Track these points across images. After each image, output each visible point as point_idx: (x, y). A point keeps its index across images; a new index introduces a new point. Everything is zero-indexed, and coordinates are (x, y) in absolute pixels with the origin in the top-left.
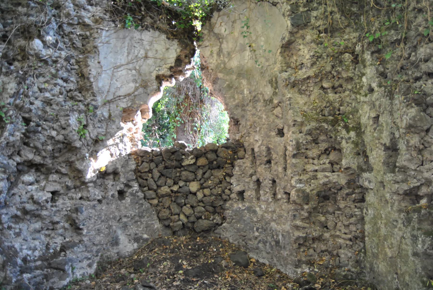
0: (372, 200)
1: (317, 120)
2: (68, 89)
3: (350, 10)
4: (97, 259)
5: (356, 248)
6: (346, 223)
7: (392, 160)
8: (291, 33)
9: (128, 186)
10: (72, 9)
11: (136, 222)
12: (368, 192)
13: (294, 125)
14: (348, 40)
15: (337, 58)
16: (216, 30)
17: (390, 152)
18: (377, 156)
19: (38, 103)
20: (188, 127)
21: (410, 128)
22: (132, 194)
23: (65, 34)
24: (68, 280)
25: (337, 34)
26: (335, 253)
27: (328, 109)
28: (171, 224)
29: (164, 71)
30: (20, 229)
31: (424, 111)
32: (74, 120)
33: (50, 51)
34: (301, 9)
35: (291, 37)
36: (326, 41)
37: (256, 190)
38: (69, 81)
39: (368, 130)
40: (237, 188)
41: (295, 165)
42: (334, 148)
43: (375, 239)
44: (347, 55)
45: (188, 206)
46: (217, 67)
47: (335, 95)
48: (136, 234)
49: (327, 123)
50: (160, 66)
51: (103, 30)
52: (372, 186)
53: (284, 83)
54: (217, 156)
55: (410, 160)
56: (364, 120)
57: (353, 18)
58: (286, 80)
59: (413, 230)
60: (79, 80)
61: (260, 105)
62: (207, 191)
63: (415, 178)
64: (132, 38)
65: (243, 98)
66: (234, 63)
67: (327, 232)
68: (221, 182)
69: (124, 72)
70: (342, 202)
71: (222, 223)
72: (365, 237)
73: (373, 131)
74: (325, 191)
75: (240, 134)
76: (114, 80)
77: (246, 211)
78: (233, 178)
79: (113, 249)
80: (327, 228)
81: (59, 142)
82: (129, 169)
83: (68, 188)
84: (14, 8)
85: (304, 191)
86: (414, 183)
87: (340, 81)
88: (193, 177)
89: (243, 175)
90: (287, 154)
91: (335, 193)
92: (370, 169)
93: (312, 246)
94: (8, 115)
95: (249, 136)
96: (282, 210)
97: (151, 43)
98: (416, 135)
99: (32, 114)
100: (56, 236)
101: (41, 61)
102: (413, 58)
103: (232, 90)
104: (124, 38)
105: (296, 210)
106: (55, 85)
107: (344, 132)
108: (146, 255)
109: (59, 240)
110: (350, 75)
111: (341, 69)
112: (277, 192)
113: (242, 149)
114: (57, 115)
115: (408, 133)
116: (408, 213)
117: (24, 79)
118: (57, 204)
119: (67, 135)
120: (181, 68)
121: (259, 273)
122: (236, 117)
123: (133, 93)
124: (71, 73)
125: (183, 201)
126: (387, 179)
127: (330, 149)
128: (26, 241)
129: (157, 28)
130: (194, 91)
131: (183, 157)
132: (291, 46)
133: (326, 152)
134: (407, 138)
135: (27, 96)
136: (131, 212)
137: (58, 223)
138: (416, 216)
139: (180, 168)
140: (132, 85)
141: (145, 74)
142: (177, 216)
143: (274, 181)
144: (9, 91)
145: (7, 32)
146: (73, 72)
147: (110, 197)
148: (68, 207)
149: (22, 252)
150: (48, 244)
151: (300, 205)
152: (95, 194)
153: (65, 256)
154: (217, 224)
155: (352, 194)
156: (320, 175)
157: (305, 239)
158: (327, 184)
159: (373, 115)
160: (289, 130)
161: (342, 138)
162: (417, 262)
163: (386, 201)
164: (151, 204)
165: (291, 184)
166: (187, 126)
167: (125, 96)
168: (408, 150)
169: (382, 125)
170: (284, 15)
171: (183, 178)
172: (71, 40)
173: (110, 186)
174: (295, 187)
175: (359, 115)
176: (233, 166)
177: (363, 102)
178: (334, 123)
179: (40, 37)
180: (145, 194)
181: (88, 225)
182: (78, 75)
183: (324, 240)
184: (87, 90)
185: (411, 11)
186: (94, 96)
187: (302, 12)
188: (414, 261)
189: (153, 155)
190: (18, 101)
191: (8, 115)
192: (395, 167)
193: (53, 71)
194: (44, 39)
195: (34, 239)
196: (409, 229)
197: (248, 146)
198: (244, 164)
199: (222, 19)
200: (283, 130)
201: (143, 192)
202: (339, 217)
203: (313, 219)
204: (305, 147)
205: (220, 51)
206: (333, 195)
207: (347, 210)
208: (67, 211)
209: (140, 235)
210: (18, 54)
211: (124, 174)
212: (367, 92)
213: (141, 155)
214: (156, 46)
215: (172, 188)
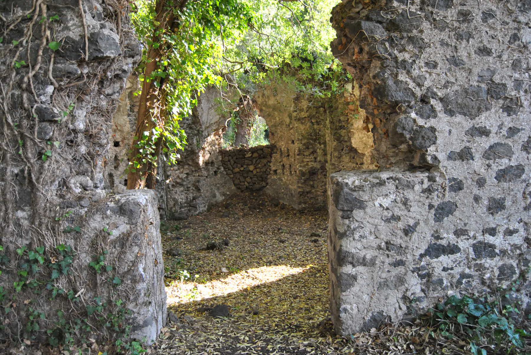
1: (308, 139)
4: (207, 204)
9: (218, 169)
20: (245, 124)
22: (221, 173)
24: (198, 212)
41: (298, 159)
42: (314, 152)
44: (322, 108)
46: (262, 103)
62: (258, 170)
68: (265, 165)
81: (189, 151)
83: (193, 171)
106: (184, 123)
107: (318, 145)
109: (191, 195)
133: (313, 153)
143: (290, 166)
157: (303, 192)
167: (214, 123)
176: (271, 157)
178: (315, 140)
198: (276, 156)
201: (226, 171)
205: (263, 95)
207: (322, 180)
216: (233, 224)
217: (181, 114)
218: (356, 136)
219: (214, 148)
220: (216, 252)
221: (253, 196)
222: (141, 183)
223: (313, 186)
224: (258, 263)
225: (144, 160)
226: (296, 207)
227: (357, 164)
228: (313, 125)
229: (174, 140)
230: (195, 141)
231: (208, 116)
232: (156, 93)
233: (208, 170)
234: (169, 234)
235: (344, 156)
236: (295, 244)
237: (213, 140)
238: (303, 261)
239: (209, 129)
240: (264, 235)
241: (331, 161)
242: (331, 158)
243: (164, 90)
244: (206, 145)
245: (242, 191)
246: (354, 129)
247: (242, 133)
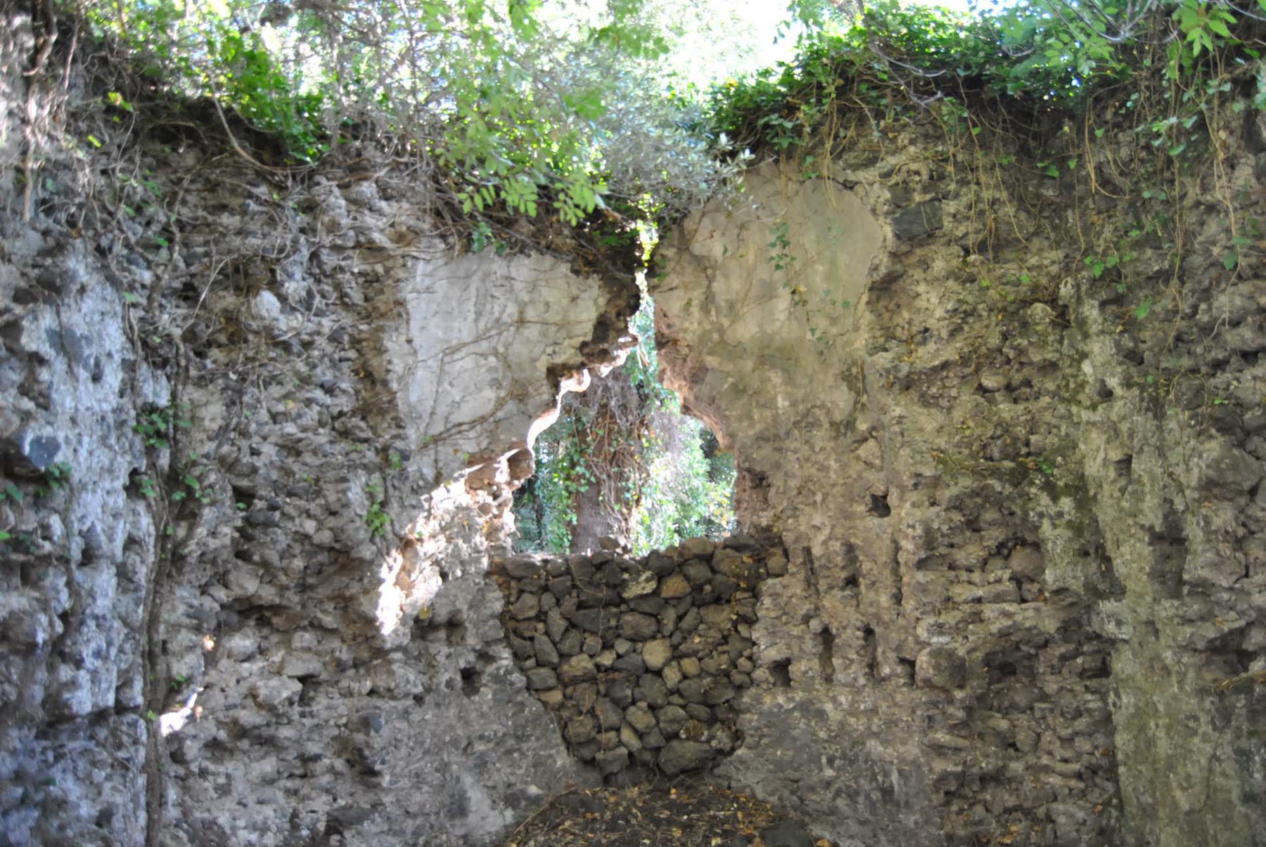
0: (1129, 670)
1: (976, 473)
2: (335, 411)
3: (1038, 196)
5: (1095, 796)
6: (1065, 733)
7: (1171, 566)
8: (894, 255)
9: (485, 656)
10: (343, 211)
11: (509, 752)
12: (1117, 650)
13: (916, 486)
14: (1039, 267)
15: (1014, 314)
16: (697, 248)
17: (1166, 547)
18: (1133, 558)
19: (269, 450)
20: (607, 493)
21: (1211, 487)
22: (496, 678)
23: (324, 273)
25: (1008, 254)
26: (1041, 812)
27: (999, 442)
28: (600, 756)
29: (567, 354)
30: (228, 776)
31: (1241, 445)
32: (359, 490)
33: (297, 321)
34: (918, 198)
35: (894, 263)
36: (984, 272)
37: (821, 657)
38: (337, 392)
39: (1107, 493)
40: (769, 653)
41: (923, 589)
42: (1022, 539)
43: (1142, 768)
44: (1039, 307)
45: (643, 705)
46: (703, 338)
47: (1013, 406)
48: (509, 785)
49: (1000, 479)
50: (556, 343)
51: (417, 258)
52: (1125, 633)
53: (883, 381)
54: (714, 571)
55: (1215, 566)
56: (1092, 468)
57: (1046, 214)
58: (888, 371)
59: (1238, 737)
60: (360, 386)
62: (690, 665)
63: (1231, 609)
64: (487, 275)
65: (775, 418)
66: (746, 330)
67: (1018, 759)
68: (725, 639)
69: (468, 363)
70: (1050, 678)
71: (733, 749)
72: (1117, 766)
73: (1117, 494)
74: (1003, 651)
75: (771, 513)
76: (446, 385)
77: (797, 714)
78: (756, 626)
79: (453, 826)
80: (1017, 750)
81: (320, 547)
82: (488, 612)
83: (341, 667)
84: (210, 219)
85: (951, 655)
86: (1230, 622)
87: (1026, 371)
88: (654, 628)
89: (784, 619)
90: (901, 560)
91: (1030, 657)
92: (1118, 591)
93: (980, 797)
94: (206, 483)
95: (796, 517)
96: (896, 705)
97: (533, 287)
98: (1225, 504)
99: (259, 480)
100: (314, 794)
101: (276, 344)
102: (1203, 318)
103: (745, 400)
105: (935, 704)
106: (309, 402)
107: (1045, 499)
108: (541, 839)
109: (321, 804)
110: (1049, 356)
111: (1025, 342)
112: (880, 658)
113: (779, 551)
114: (317, 480)
115: (1206, 499)
116: (1221, 695)
117: (240, 393)
118: (315, 708)
119: (342, 530)
120: (606, 346)
122: (758, 468)
123: (493, 414)
124: (340, 370)
125: (629, 692)
126: (1164, 614)
127: (1010, 544)
128: (245, 806)
129: (548, 247)
130: (624, 396)
131: (626, 576)
132: (894, 287)
133: (1002, 551)
134: (1204, 511)
135: (244, 434)
136: (495, 727)
137: (317, 758)
138: (1241, 702)
139: (618, 606)
140: (490, 394)
141: (520, 365)
142: (612, 734)
143: (869, 632)
144: (207, 423)
145: (193, 276)
146: (345, 365)
147: (443, 687)
148: (341, 716)
149: (235, 834)
150: (295, 815)
151: (945, 690)
152: (408, 681)
154: (720, 752)
155: (1075, 657)
156: (989, 611)
157: (962, 779)
158: (1008, 634)
159: (1115, 455)
160: (902, 499)
161: (1041, 515)
162: (1254, 816)
163: (1166, 670)
164: (545, 704)
165: (916, 638)
166: (604, 491)
167: (473, 424)
168: (1208, 541)
169: (1139, 481)
170: (874, 211)
171: (628, 631)
172: (338, 286)
173: (441, 659)
175: (1078, 456)
176: (756, 595)
177: (1088, 423)
178: (1019, 477)
179: (274, 285)
180: (528, 678)
181: (392, 762)
182: (357, 374)
183: (1010, 780)
184: (382, 412)
185: (1190, 208)
186: (399, 427)
187: (919, 204)
188: (1247, 816)
189: (548, 573)
190: (226, 449)
191: (206, 483)
192: (1181, 582)
193: (302, 367)
194: (283, 291)
195: (261, 802)
196: (1229, 735)
197: (797, 540)
198: (783, 591)
199: (713, 222)
200: (885, 497)
201: (522, 670)
202: (1044, 718)
203: (979, 726)
204: (946, 541)
205: (709, 299)
206: (1026, 662)
207: (1066, 700)
208: (338, 727)
209: (519, 786)
210: (219, 331)
211: (475, 625)
212: (1097, 398)
213: (517, 573)
214: (545, 292)
215: (598, 659)
221: (671, 806)
230: (355, 493)
239: (445, 451)
244: (423, 527)
245: (607, 780)
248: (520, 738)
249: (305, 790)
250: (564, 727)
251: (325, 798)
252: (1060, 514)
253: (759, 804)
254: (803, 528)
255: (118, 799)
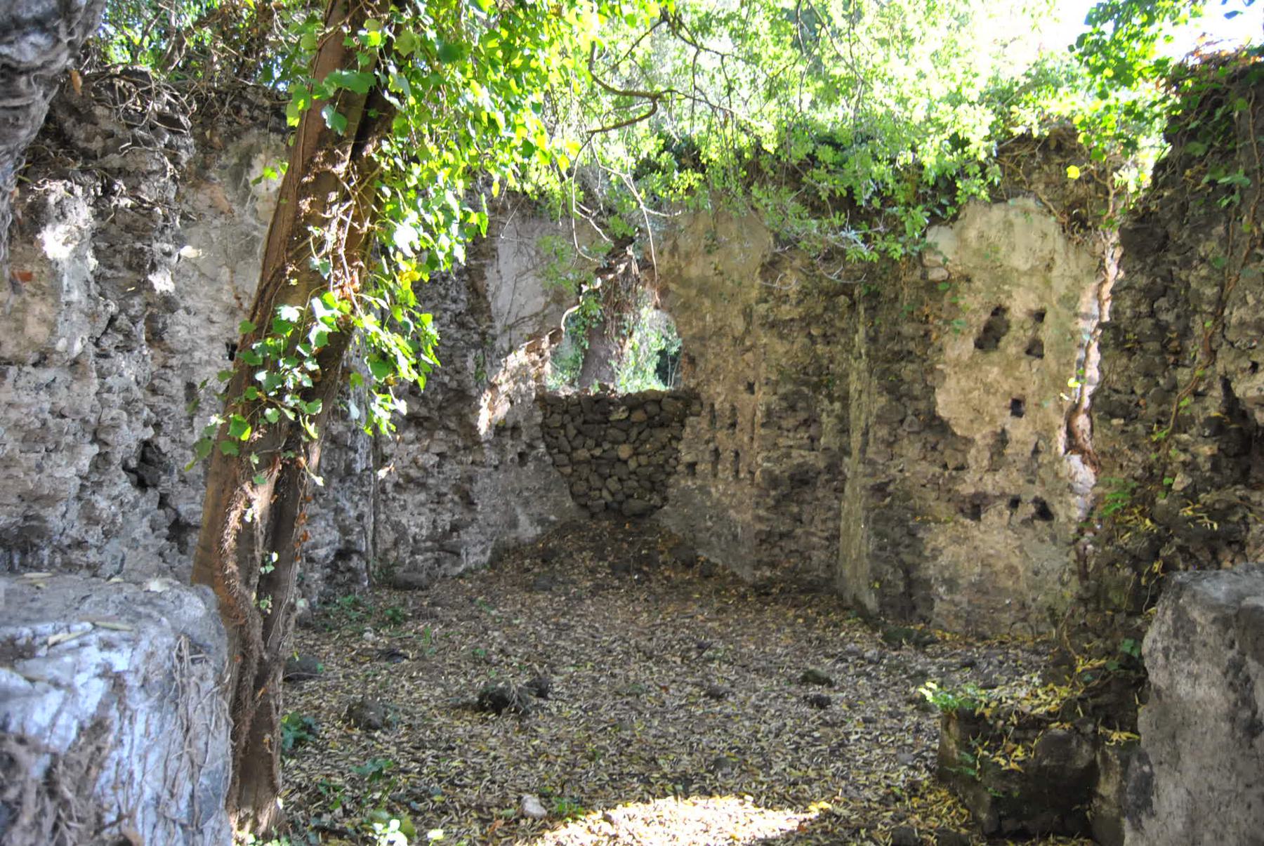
1: (795, 382)
4: (491, 544)
9: (531, 446)
11: (541, 497)
20: (610, 329)
21: (880, 419)
24: (463, 566)
28: (589, 503)
40: (687, 458)
41: (763, 438)
44: (842, 298)
45: (615, 478)
61: (726, 342)
62: (643, 460)
65: (705, 326)
66: (694, 271)
81: (451, 389)
83: (457, 449)
86: (882, 479)
103: (689, 313)
104: (533, 231)
106: (445, 310)
107: (826, 402)
109: (447, 517)
114: (451, 355)
121: (707, 573)
133: (806, 423)
137: (445, 494)
142: (597, 493)
143: (737, 454)
150: (435, 521)
153: (459, 536)
154: (655, 507)
156: (795, 453)
157: (769, 534)
167: (530, 318)
173: (508, 447)
174: (761, 466)
176: (683, 426)
178: (816, 388)
184: (482, 312)
198: (697, 424)
201: (550, 454)
216: (564, 615)
217: (427, 258)
218: (951, 383)
219: (523, 386)
220: (509, 723)
221: (625, 532)
222: (251, 495)
223: (798, 519)
224: (646, 781)
225: (269, 411)
226: (746, 574)
227: (945, 466)
228: (814, 342)
229: (391, 345)
230: (470, 363)
231: (513, 289)
232: (340, 169)
233: (502, 450)
234: (369, 635)
235: (906, 441)
236: (757, 708)
237: (521, 365)
238: (795, 784)
239: (515, 333)
240: (657, 663)
241: (863, 451)
242: (866, 443)
243: (372, 165)
244: (501, 377)
245: (593, 516)
246: (945, 363)
247: (602, 353)
248: (548, 490)
249: (440, 510)
250: (571, 486)
251: (449, 514)
252: (833, 411)
253: (671, 535)
254: (712, 392)
255: (366, 509)
